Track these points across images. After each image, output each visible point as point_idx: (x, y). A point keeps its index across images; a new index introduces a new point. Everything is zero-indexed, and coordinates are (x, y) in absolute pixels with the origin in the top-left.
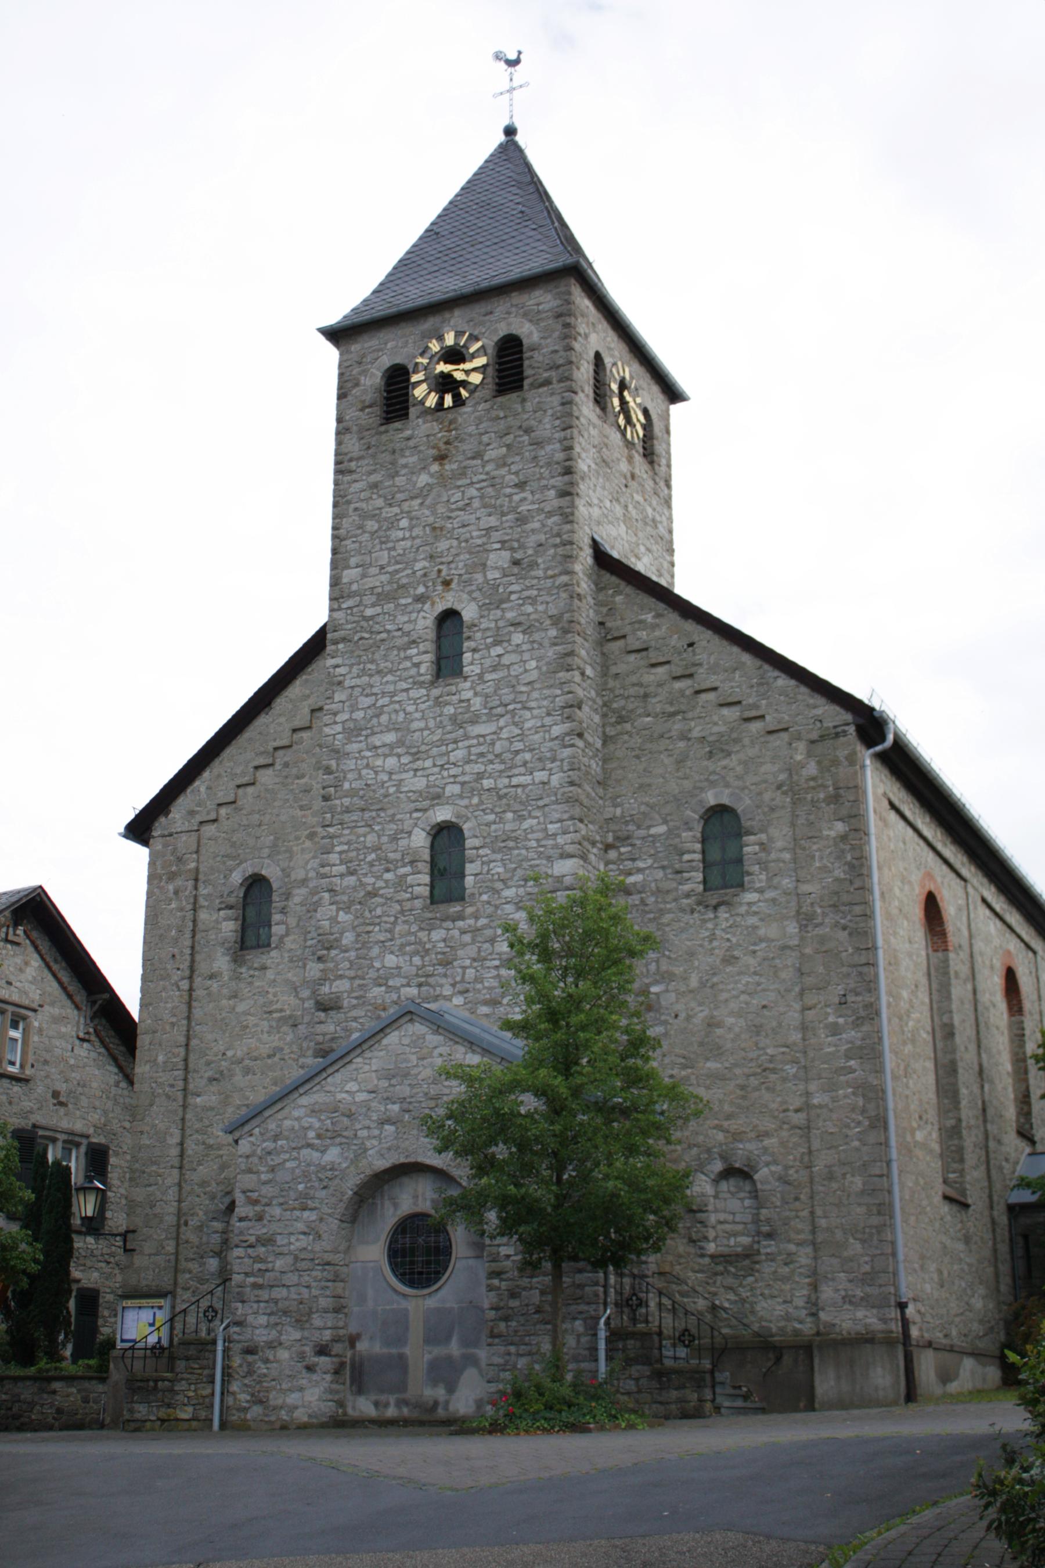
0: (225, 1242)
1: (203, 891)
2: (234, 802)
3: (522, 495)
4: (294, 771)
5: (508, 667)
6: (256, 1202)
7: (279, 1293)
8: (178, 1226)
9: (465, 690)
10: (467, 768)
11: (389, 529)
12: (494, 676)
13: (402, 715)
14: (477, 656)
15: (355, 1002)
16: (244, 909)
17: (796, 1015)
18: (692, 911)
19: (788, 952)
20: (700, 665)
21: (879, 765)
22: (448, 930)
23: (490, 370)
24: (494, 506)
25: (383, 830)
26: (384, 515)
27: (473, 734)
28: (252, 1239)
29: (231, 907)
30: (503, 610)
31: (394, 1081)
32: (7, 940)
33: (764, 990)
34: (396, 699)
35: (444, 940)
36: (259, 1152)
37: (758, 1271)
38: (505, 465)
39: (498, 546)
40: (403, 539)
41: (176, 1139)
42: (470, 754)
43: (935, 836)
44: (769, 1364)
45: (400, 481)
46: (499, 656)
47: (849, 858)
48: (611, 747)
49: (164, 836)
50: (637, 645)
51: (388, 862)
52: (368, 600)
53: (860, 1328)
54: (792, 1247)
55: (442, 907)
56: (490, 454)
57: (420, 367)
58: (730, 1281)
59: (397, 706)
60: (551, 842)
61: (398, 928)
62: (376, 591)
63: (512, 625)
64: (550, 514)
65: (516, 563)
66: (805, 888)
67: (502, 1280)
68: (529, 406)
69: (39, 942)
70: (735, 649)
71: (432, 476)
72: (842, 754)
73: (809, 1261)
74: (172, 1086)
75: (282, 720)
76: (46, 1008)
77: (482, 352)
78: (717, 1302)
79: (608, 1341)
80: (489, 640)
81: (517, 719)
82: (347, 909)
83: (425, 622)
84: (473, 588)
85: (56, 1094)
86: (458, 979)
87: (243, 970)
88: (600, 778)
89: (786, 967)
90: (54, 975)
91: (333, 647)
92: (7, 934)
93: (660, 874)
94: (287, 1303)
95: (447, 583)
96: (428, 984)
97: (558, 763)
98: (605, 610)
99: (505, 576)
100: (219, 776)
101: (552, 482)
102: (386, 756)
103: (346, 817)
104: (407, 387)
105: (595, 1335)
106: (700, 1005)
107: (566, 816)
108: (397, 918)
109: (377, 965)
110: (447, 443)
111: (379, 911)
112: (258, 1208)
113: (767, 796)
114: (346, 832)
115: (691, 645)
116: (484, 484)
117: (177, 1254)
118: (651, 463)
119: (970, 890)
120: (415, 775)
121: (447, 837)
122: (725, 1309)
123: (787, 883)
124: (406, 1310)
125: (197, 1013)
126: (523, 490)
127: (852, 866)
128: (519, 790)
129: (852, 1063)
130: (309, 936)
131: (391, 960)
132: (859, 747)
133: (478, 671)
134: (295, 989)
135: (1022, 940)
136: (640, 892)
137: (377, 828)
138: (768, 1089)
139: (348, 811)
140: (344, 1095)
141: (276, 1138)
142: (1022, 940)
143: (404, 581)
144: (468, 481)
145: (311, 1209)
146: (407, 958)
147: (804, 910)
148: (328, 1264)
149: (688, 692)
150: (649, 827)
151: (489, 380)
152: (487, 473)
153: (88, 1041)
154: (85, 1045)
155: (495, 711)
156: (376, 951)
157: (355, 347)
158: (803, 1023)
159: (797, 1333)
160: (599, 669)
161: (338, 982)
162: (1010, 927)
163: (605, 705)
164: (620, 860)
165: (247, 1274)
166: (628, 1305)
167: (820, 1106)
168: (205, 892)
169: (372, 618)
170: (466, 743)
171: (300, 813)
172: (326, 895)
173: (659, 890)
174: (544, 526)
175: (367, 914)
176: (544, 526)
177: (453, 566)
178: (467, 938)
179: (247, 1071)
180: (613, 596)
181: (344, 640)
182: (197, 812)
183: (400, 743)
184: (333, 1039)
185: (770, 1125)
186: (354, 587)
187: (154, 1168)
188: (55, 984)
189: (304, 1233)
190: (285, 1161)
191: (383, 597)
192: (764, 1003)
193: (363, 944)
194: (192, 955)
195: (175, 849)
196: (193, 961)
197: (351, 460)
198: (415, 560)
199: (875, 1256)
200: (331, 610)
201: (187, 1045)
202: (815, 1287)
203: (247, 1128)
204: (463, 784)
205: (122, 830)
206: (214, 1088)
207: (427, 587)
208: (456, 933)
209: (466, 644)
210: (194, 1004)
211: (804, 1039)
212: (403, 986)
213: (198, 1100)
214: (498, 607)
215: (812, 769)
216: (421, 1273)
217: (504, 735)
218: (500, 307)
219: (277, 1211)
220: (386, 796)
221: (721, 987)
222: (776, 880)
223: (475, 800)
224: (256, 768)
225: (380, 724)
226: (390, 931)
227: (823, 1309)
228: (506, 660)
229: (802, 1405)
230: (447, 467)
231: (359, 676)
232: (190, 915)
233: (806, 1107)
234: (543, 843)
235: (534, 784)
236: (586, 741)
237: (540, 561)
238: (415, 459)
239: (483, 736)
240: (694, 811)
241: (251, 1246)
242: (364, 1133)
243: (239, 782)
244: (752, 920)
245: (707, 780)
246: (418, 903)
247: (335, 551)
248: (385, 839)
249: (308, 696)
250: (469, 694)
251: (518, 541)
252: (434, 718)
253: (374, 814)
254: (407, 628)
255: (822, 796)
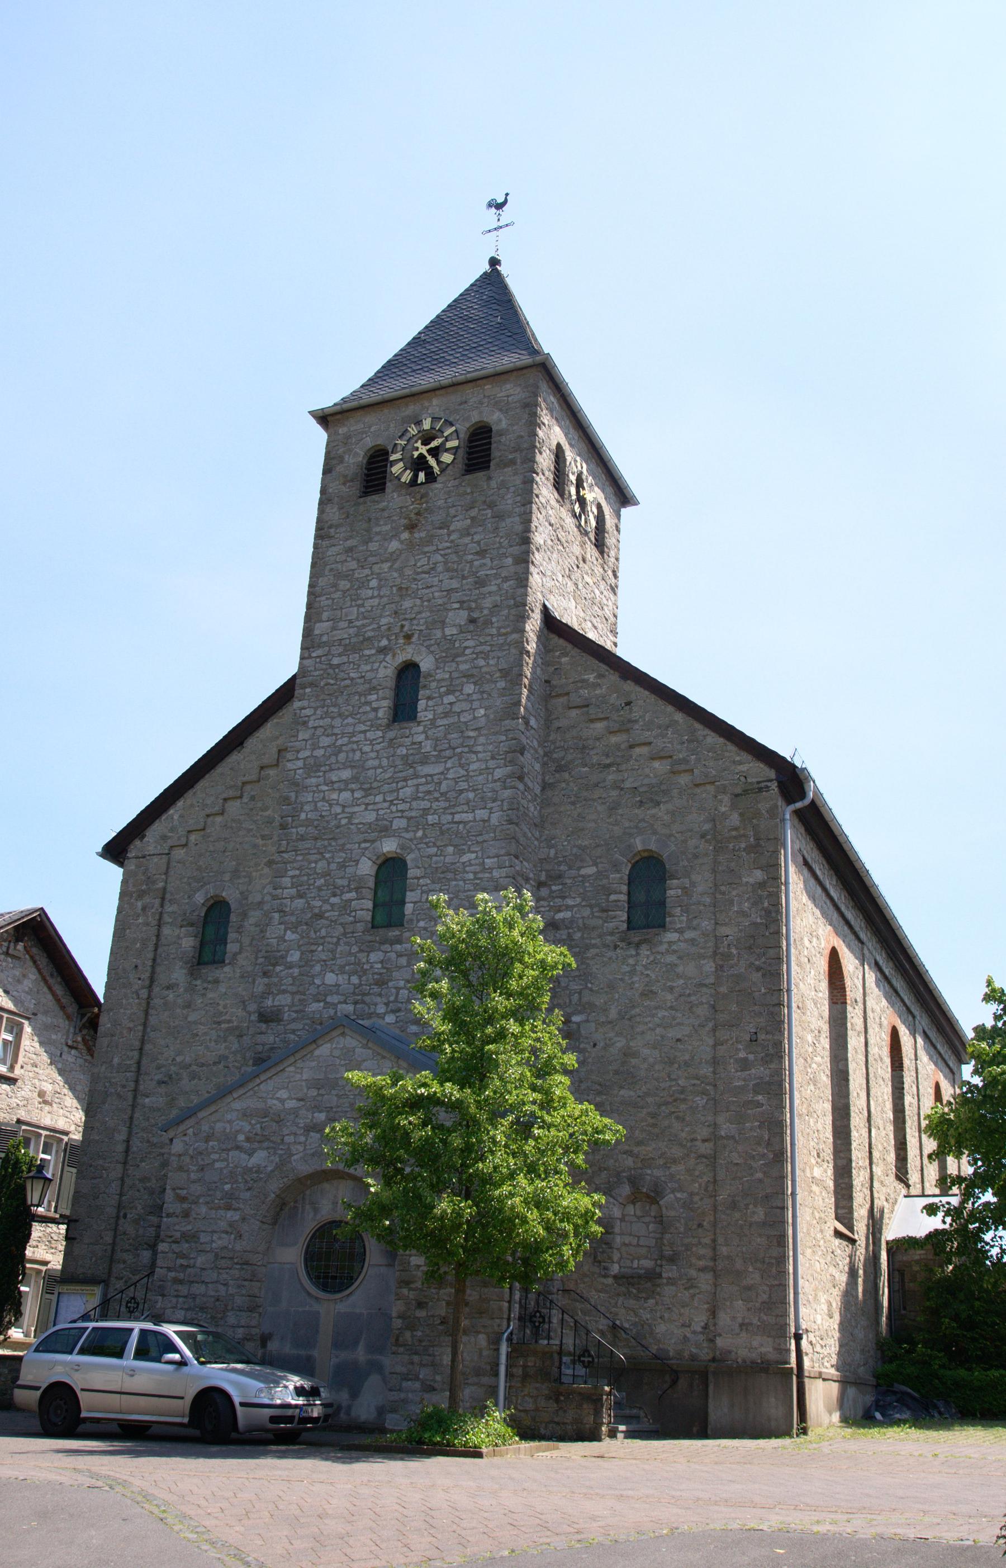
0: (158, 1236)
1: (169, 908)
2: (204, 829)
3: (484, 561)
4: (259, 804)
5: (459, 714)
6: (183, 1199)
7: (198, 1289)
8: (118, 1217)
9: (417, 732)
10: (414, 804)
11: (359, 588)
12: (445, 722)
13: (358, 754)
14: (430, 703)
15: (295, 1015)
16: (204, 926)
17: (708, 1049)
18: (616, 947)
19: (704, 990)
20: (636, 721)
21: (796, 821)
22: (387, 952)
23: (461, 453)
24: (456, 571)
25: (333, 857)
26: (356, 575)
27: (422, 773)
28: (178, 1235)
29: (192, 925)
30: (457, 663)
31: (322, 1092)
32: (7, 954)
33: (679, 1024)
34: (354, 739)
35: (382, 962)
36: (191, 1152)
37: (659, 1294)
38: (468, 534)
39: (457, 606)
40: (372, 597)
41: (122, 1136)
42: (418, 792)
43: (840, 898)
44: (666, 1386)
45: (373, 546)
46: (451, 704)
47: (766, 904)
48: (549, 793)
49: (137, 857)
50: (578, 701)
51: (335, 888)
52: (337, 650)
53: (754, 1356)
54: (693, 1273)
55: (382, 931)
56: (457, 525)
57: (399, 448)
58: (631, 1303)
59: (355, 746)
60: (487, 875)
61: (339, 949)
62: (343, 642)
63: (464, 677)
64: (506, 579)
65: (472, 621)
66: (724, 930)
67: (410, 1289)
68: (493, 484)
69: (37, 958)
70: (670, 709)
71: (402, 542)
72: (763, 807)
73: (709, 1288)
74: (124, 1086)
75: (253, 757)
76: (39, 1016)
77: (455, 436)
78: (618, 1322)
79: (509, 1355)
80: (442, 690)
81: (463, 761)
82: (294, 927)
83: (386, 671)
84: (432, 642)
85: (41, 1094)
86: (392, 998)
87: (198, 982)
88: (537, 821)
89: (702, 1003)
90: (50, 988)
91: (301, 691)
92: (8, 948)
93: (587, 912)
94: (205, 1299)
95: (408, 637)
96: (363, 1002)
97: (499, 803)
98: (551, 669)
99: (461, 632)
100: (192, 806)
101: (510, 550)
102: (341, 791)
103: (301, 845)
104: (386, 466)
105: (497, 1350)
106: (617, 1035)
107: (502, 852)
108: (339, 939)
109: (317, 981)
110: (418, 514)
111: (323, 932)
112: (185, 1206)
113: (692, 843)
114: (300, 858)
115: (628, 704)
116: (450, 551)
117: (114, 1244)
118: (602, 553)
119: (866, 951)
120: (366, 809)
121: (392, 871)
122: (624, 1330)
123: (706, 924)
124: (318, 1313)
125: (153, 1020)
126: (484, 557)
127: (768, 912)
128: (461, 826)
129: (760, 1097)
130: (260, 955)
131: (330, 978)
132: (780, 802)
133: (431, 717)
134: (244, 1002)
135: (905, 1004)
136: (567, 928)
137: (327, 856)
138: (677, 1118)
139: (302, 838)
140: (275, 1102)
141: (207, 1139)
142: (905, 1004)
143: (370, 634)
144: (435, 548)
145: (235, 1210)
146: (346, 977)
147: (721, 950)
148: (247, 1263)
149: (623, 746)
150: (579, 869)
151: (460, 459)
152: (452, 542)
153: (76, 1048)
154: (73, 1052)
155: (443, 754)
156: (318, 968)
157: (342, 430)
158: (714, 1058)
159: (693, 1358)
160: (542, 722)
161: (280, 997)
162: (896, 991)
163: (546, 754)
164: (552, 896)
165: (169, 1269)
166: (531, 1321)
167: (728, 1137)
168: (170, 909)
169: (338, 666)
170: (415, 782)
171: (260, 842)
172: (276, 915)
173: (586, 927)
174: (500, 589)
175: (312, 935)
176: (500, 589)
177: (415, 622)
178: (403, 961)
179: (193, 1076)
180: (559, 657)
181: (311, 685)
182: (170, 837)
183: (355, 779)
184: (272, 1049)
185: (677, 1152)
186: (325, 639)
187: (101, 1162)
188: (50, 997)
189: (227, 1233)
190: (214, 1161)
191: (350, 648)
192: (679, 1037)
193: (306, 963)
194: (153, 967)
195: (147, 869)
196: (153, 972)
197: (330, 527)
198: (381, 616)
199: (773, 1286)
200: (302, 658)
201: (141, 1049)
202: (713, 1313)
203: (182, 1128)
204: (409, 819)
205: (100, 850)
206: (162, 1089)
207: (389, 640)
208: (393, 955)
209: (421, 693)
210: (151, 1011)
211: (714, 1073)
212: (340, 1003)
213: (147, 1100)
214: (453, 661)
215: (735, 819)
216: (334, 1278)
217: (451, 775)
218: (473, 395)
219: (204, 1209)
220: (338, 827)
221: (638, 1019)
222: (695, 923)
223: (420, 834)
224: (225, 800)
225: (337, 762)
226: (333, 951)
227: (720, 1335)
228: (456, 708)
229: (695, 1429)
230: (416, 535)
231: (322, 718)
232: (154, 930)
233: (714, 1138)
234: (480, 875)
235: (475, 821)
236: (526, 785)
237: (494, 620)
238: (388, 527)
239: (431, 776)
240: (623, 856)
241: (176, 1242)
242: (292, 1139)
243: (208, 811)
244: (671, 959)
245: (637, 827)
246: (360, 927)
247: (309, 606)
248: (333, 866)
249: (278, 738)
250: (422, 737)
251: (475, 601)
252: (388, 758)
253: (326, 843)
254: (369, 676)
255: (743, 845)
